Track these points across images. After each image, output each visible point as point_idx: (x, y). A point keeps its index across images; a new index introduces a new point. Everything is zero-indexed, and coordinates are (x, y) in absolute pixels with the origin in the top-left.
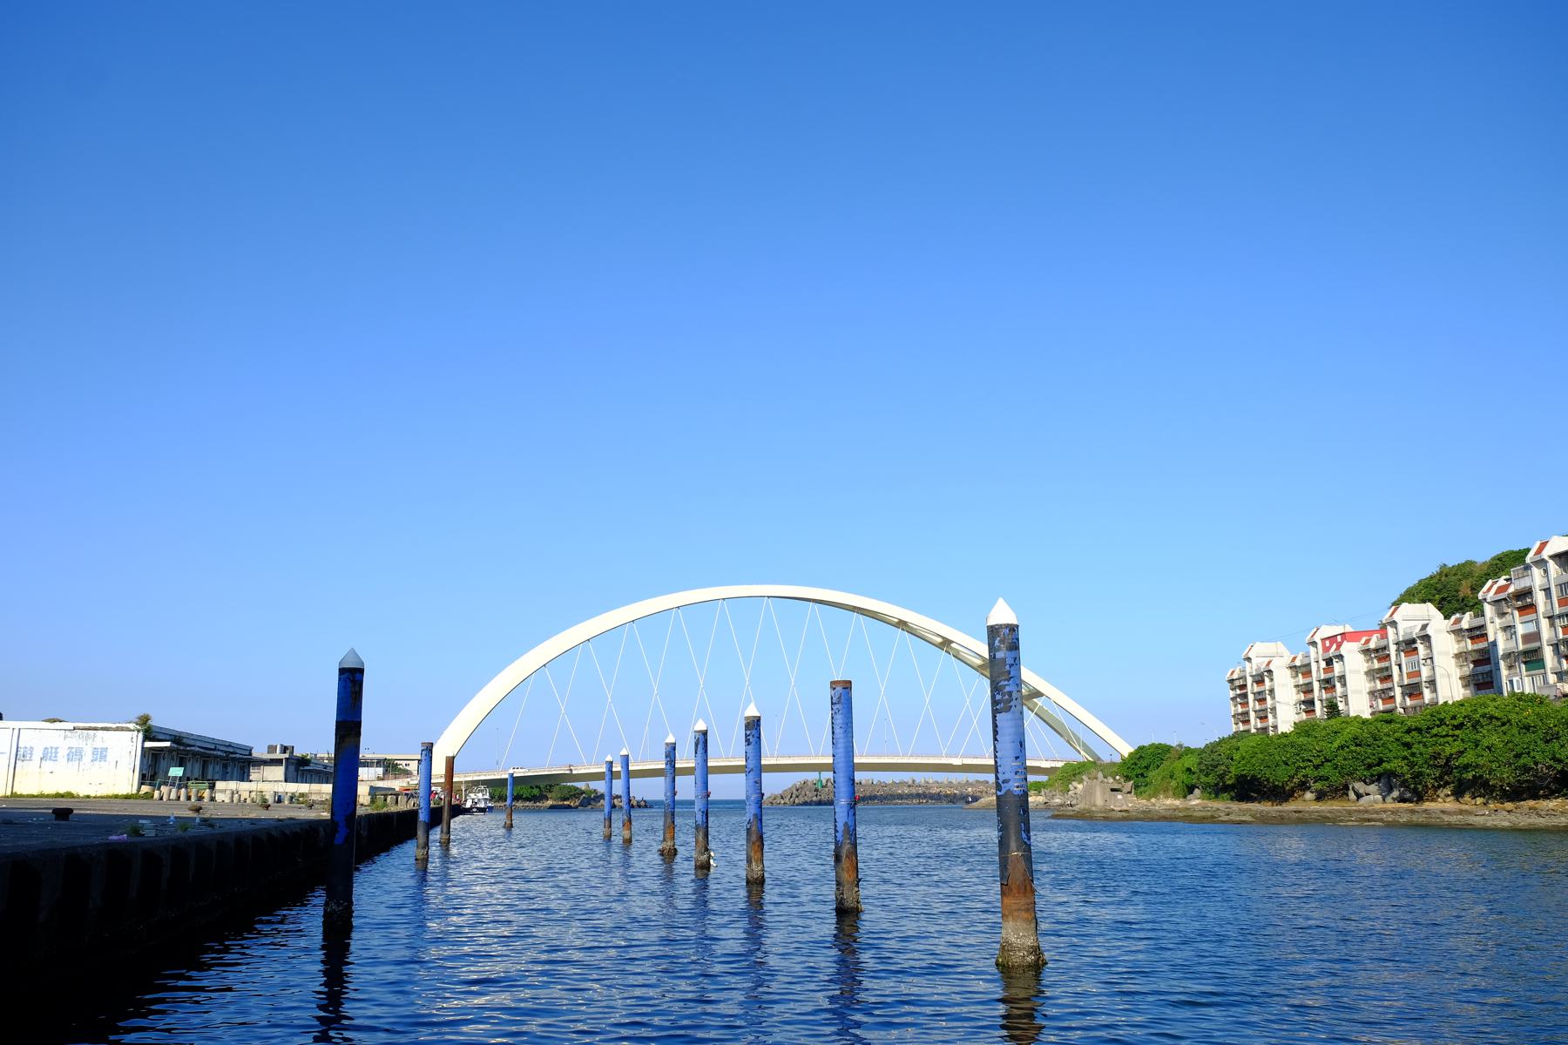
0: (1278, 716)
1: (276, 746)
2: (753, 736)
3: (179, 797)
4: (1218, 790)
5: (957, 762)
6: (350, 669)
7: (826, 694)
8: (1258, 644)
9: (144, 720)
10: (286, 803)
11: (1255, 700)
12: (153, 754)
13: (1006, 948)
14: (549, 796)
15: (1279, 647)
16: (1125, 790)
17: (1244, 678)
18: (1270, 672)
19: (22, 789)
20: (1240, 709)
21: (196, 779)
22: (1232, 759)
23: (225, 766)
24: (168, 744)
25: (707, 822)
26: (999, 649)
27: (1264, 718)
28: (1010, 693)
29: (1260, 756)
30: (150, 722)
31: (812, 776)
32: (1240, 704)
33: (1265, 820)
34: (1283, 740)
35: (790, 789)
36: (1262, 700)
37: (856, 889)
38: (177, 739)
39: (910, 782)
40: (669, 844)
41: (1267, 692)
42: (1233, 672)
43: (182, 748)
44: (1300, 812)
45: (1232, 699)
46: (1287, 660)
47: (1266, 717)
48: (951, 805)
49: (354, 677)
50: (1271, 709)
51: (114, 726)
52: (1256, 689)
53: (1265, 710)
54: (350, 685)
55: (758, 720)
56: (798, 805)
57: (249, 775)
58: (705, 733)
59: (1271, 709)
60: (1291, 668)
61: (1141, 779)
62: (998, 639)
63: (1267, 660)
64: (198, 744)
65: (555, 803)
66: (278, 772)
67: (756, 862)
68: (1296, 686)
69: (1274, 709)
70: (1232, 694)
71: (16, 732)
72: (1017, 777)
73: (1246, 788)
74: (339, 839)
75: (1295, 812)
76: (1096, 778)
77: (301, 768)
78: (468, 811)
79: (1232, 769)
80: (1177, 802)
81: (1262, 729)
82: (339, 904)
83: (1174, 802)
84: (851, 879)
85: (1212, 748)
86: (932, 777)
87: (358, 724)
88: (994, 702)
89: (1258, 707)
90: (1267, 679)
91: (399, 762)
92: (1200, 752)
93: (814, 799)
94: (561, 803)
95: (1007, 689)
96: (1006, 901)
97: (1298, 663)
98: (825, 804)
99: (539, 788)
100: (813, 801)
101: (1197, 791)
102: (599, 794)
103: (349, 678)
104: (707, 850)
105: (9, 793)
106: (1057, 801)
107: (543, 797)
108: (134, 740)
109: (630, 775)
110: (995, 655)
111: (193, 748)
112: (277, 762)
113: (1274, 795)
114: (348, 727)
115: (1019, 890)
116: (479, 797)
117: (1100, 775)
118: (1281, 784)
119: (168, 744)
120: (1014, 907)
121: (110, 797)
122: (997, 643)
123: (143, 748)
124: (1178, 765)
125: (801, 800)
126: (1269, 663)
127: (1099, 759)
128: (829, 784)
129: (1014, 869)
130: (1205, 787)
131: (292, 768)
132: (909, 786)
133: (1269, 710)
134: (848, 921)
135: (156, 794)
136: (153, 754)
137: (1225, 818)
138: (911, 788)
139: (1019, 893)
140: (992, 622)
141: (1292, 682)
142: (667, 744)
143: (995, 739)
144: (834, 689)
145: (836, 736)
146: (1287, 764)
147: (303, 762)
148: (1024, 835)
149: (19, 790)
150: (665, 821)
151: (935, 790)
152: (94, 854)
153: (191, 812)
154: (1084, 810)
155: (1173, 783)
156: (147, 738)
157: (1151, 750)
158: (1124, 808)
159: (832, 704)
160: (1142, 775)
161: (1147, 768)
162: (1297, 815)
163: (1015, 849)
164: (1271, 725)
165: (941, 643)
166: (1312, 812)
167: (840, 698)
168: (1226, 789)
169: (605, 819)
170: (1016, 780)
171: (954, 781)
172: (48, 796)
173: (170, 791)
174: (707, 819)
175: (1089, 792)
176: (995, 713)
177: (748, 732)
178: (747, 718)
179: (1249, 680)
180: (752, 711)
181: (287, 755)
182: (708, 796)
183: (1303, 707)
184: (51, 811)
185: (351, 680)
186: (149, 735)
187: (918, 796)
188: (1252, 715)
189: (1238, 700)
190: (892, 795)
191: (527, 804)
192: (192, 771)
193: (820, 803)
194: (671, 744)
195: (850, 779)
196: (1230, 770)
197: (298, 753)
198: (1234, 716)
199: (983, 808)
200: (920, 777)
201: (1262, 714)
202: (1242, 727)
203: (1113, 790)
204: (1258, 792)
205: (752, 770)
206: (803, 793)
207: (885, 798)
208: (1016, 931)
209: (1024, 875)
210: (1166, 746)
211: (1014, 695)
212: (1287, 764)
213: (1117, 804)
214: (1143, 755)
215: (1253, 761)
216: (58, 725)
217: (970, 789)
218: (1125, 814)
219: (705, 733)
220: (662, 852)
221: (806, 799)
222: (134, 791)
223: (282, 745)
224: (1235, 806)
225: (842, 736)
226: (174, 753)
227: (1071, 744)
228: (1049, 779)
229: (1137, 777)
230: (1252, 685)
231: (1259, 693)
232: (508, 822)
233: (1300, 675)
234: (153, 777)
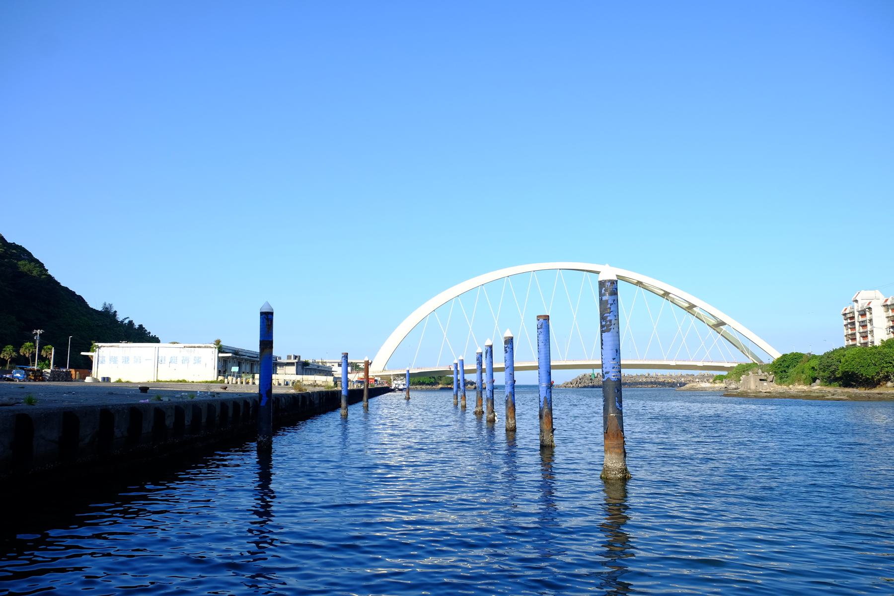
0: (875, 335)
1: (291, 356)
2: (509, 348)
3: (237, 382)
4: (831, 380)
5: (673, 363)
6: (265, 312)
7: (535, 323)
8: (863, 292)
9: (218, 342)
10: (291, 385)
11: (860, 326)
12: (224, 360)
13: (606, 470)
14: (440, 383)
15: (878, 294)
16: (769, 380)
17: (853, 313)
18: (870, 309)
19: (162, 378)
20: (850, 332)
21: (248, 373)
22: (840, 362)
23: (252, 365)
24: (230, 355)
25: (493, 396)
26: (604, 295)
27: (865, 337)
28: (610, 321)
29: (857, 360)
30: (221, 343)
31: (589, 372)
32: (850, 328)
33: (856, 398)
34: (873, 350)
35: (576, 379)
36: (865, 326)
37: (551, 434)
38: (236, 352)
39: (647, 375)
40: (479, 408)
41: (868, 321)
42: (846, 309)
43: (238, 356)
44: (881, 394)
45: (845, 325)
46: (882, 302)
47: (867, 336)
48: (671, 388)
49: (268, 317)
50: (870, 332)
51: (203, 345)
52: (861, 319)
53: (866, 332)
54: (266, 321)
55: (512, 339)
56: (580, 388)
57: (276, 371)
58: (491, 347)
59: (870, 332)
60: (884, 306)
61: (784, 373)
62: (604, 289)
63: (869, 301)
64: (248, 355)
65: (443, 386)
66: (293, 369)
67: (511, 418)
68: (888, 317)
69: (872, 331)
70: (845, 322)
71: (157, 348)
72: (614, 370)
73: (849, 379)
74: (263, 403)
75: (878, 394)
76: (757, 373)
77: (305, 367)
78: (393, 390)
79: (840, 368)
80: (805, 388)
81: (864, 343)
82: (264, 438)
83: (803, 387)
84: (548, 429)
85: (828, 355)
86: (660, 372)
87: (271, 343)
88: (602, 326)
89: (861, 330)
90: (868, 313)
91: (359, 364)
92: (822, 357)
93: (590, 384)
94: (447, 386)
95: (609, 318)
96: (607, 442)
97: (889, 303)
98: (596, 387)
99: (434, 378)
100: (585, 386)
101: (818, 381)
102: (467, 381)
103: (265, 317)
104: (493, 412)
105: (155, 380)
106: (733, 386)
107: (436, 383)
108: (214, 353)
109: (464, 372)
110: (602, 298)
111: (244, 357)
112: (292, 364)
113: (867, 384)
114: (267, 342)
115: (613, 436)
116: (401, 383)
117: (760, 371)
118: (870, 377)
119: (230, 355)
120: (610, 446)
121: (204, 382)
122: (603, 291)
123: (218, 357)
124: (807, 365)
125: (583, 385)
126: (870, 303)
127: (761, 362)
128: (599, 376)
129: (611, 424)
130: (823, 378)
131: (300, 367)
132: (646, 377)
133: (869, 332)
134: (547, 452)
135: (226, 381)
136: (224, 360)
137: (830, 397)
138: (647, 379)
139: (614, 438)
140: (600, 280)
141: (885, 315)
142: (477, 353)
143: (602, 348)
144: (539, 320)
145: (540, 347)
146: (875, 365)
147: (306, 364)
148: (617, 404)
149: (160, 379)
150: (477, 396)
151: (661, 380)
152: (120, 409)
153: (222, 390)
154: (743, 391)
155: (804, 376)
156: (220, 351)
157: (791, 356)
158: (768, 390)
159: (538, 329)
160: (785, 371)
161: (788, 367)
162: (879, 396)
163: (611, 412)
164: (869, 341)
165: (663, 294)
166: (890, 394)
167: (542, 325)
168: (836, 379)
169: (454, 395)
170: (613, 372)
171: (673, 375)
172: (174, 382)
173: (233, 379)
174: (493, 394)
175: (747, 382)
176: (602, 332)
177: (506, 346)
178: (505, 338)
179: (856, 314)
180: (508, 334)
181: (296, 361)
182: (493, 382)
183: (891, 330)
184: (138, 388)
185: (267, 318)
186: (221, 350)
187: (652, 383)
188: (858, 335)
189: (849, 326)
190: (635, 383)
191: (428, 387)
192: (245, 369)
193: (593, 387)
194: (480, 353)
195: (548, 372)
196: (839, 368)
197: (303, 359)
198: (846, 336)
199: (687, 390)
200: (653, 372)
201: (864, 335)
202: (851, 342)
203: (761, 380)
204: (856, 381)
205: (508, 367)
206: (584, 381)
207: (632, 384)
208: (611, 459)
209: (617, 428)
210: (800, 354)
211: (613, 322)
212: (875, 365)
213: (764, 388)
214: (785, 359)
215: (853, 363)
216: (176, 345)
217: (683, 379)
218: (768, 394)
219: (491, 347)
220: (475, 413)
221: (585, 385)
222: (215, 380)
223: (294, 355)
224: (840, 390)
225: (543, 347)
226: (235, 359)
227: (744, 354)
228: (728, 374)
229: (782, 372)
230: (858, 317)
231: (863, 322)
232: (407, 396)
233: (890, 311)
234: (225, 372)
